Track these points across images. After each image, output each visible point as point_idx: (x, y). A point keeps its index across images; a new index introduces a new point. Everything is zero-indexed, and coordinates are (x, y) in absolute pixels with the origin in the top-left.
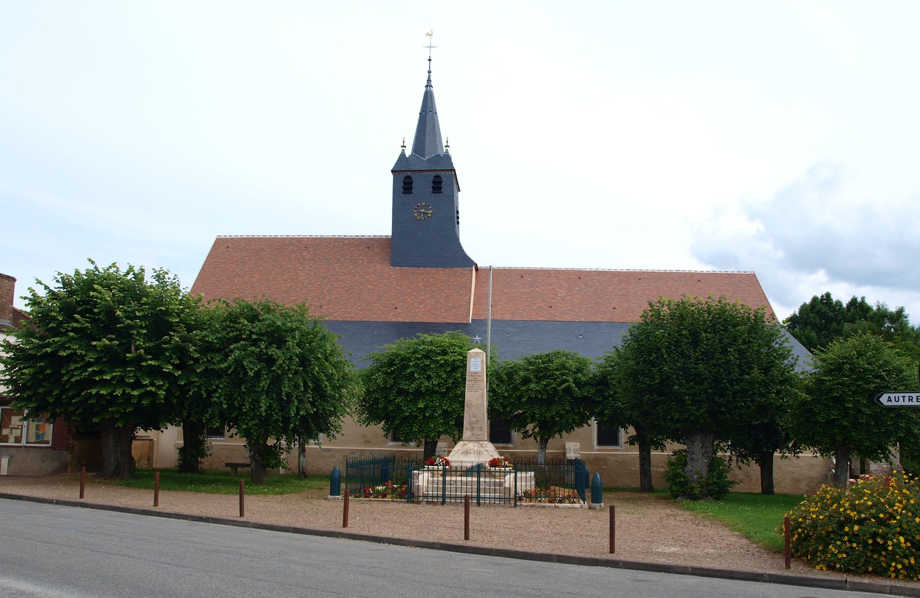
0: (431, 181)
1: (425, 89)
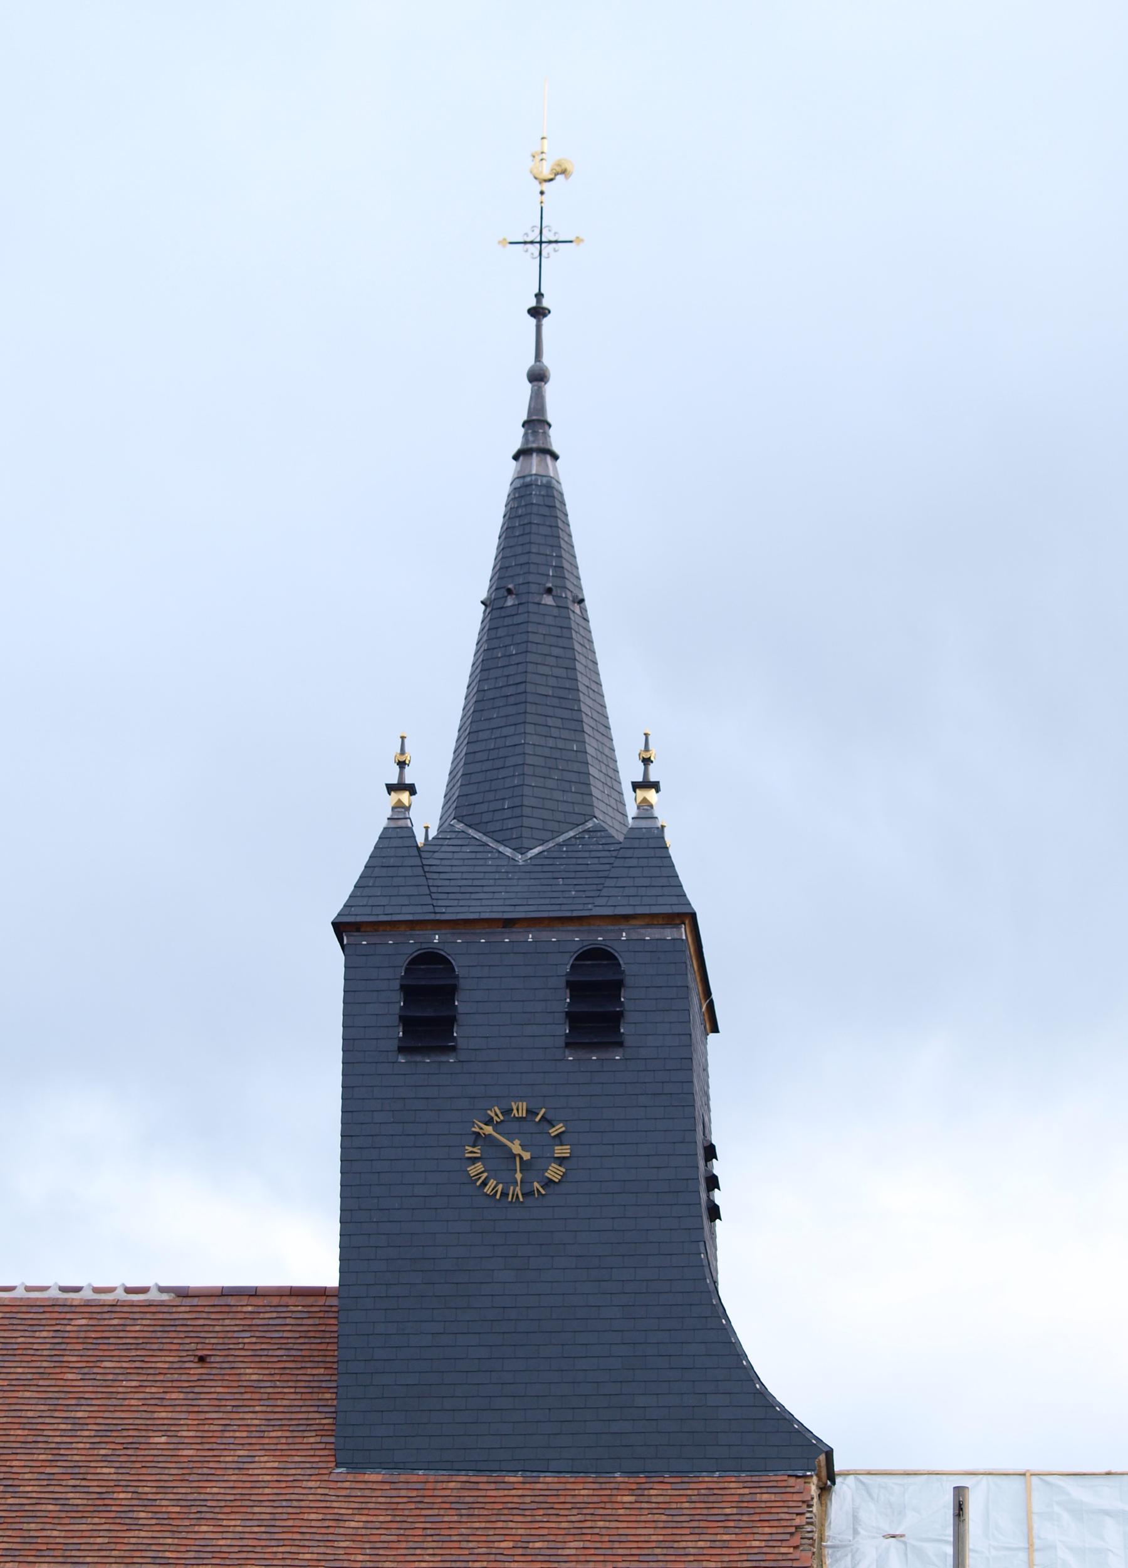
0: (562, 982)
1: (509, 469)
